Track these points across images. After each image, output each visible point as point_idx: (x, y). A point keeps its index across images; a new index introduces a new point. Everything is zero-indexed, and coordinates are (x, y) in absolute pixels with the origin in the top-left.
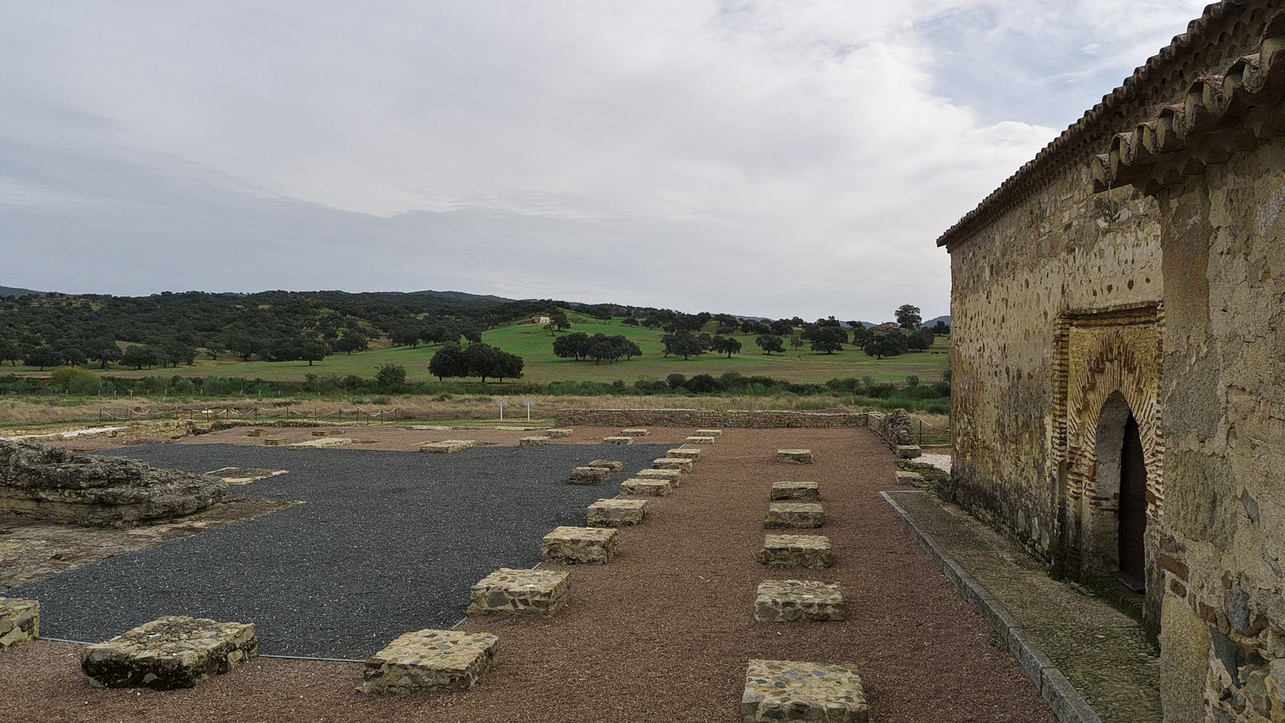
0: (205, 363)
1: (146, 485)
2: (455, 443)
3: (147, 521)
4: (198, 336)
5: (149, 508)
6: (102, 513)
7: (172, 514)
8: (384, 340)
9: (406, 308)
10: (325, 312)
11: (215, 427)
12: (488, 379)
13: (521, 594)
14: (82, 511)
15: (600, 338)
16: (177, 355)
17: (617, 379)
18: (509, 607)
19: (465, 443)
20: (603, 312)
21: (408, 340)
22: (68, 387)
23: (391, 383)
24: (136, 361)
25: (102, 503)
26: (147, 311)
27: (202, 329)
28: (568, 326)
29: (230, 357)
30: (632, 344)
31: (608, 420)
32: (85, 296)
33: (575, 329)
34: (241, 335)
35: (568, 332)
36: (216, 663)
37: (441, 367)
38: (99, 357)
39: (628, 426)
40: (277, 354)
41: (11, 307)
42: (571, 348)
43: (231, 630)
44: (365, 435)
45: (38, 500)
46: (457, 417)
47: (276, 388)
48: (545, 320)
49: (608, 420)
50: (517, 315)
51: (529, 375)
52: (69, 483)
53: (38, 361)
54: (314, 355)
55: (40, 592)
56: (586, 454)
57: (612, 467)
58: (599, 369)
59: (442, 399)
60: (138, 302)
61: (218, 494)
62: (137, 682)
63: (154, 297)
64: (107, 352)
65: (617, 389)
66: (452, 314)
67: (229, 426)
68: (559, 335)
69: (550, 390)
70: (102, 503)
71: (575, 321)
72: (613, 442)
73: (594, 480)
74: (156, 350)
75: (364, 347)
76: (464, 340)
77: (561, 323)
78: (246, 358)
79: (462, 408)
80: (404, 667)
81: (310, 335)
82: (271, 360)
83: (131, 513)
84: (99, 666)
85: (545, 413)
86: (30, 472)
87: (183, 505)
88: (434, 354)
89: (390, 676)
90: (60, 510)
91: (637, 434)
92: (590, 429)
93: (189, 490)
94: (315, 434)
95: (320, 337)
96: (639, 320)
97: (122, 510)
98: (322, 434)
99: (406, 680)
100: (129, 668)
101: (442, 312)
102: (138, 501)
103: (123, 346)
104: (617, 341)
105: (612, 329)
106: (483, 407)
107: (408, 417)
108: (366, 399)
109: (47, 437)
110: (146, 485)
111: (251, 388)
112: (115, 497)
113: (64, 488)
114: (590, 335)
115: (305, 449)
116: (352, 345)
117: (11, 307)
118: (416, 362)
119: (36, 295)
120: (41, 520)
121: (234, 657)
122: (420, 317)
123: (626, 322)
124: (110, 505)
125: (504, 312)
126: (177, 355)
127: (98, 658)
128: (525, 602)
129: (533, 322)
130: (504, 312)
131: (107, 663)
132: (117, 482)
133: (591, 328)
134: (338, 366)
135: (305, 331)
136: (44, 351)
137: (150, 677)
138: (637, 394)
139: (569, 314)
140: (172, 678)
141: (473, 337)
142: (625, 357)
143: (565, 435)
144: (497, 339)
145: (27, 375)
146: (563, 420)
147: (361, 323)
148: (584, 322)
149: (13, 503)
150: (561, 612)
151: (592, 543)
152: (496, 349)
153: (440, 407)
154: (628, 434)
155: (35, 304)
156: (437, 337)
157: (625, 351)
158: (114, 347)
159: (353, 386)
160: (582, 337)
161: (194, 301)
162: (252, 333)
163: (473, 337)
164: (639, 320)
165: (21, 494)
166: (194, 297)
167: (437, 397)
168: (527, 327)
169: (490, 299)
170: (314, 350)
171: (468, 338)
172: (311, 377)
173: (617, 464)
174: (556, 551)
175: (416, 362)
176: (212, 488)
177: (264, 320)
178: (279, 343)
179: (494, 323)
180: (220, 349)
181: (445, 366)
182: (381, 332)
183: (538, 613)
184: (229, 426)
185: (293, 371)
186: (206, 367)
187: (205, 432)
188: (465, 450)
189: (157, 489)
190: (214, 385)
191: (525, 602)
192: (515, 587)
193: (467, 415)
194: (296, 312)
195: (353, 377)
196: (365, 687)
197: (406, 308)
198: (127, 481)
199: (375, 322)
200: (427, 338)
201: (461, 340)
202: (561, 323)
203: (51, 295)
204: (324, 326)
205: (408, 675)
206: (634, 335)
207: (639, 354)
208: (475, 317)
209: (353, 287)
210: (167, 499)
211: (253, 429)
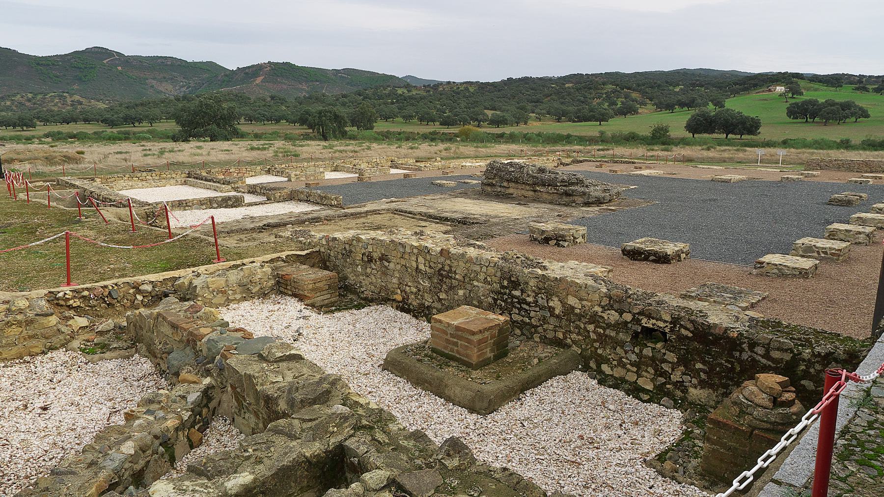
0: (535, 123)
1: (587, 186)
2: (735, 177)
3: (588, 204)
4: (529, 106)
5: (589, 198)
6: (566, 199)
7: (599, 202)
8: (649, 106)
9: (667, 82)
10: (610, 87)
11: (573, 162)
12: (730, 136)
13: (823, 248)
14: (556, 197)
15: (830, 103)
16: (519, 119)
17: (844, 138)
18: (815, 254)
19: (741, 177)
20: (835, 81)
21: (670, 107)
22: (466, 137)
23: (659, 138)
24: (497, 122)
25: (567, 194)
26: (499, 91)
27: (532, 102)
28: (801, 94)
29: (549, 120)
30: (861, 109)
31: (849, 167)
32: (464, 83)
33: (807, 96)
34: (556, 105)
35: (800, 99)
36: (677, 256)
37: (695, 127)
38: (477, 120)
39: (866, 172)
40: (578, 117)
41: (429, 91)
42: (803, 112)
43: (680, 246)
44: (669, 170)
45: (535, 191)
46: (725, 161)
47: (582, 140)
48: (780, 89)
49: (849, 167)
50: (755, 86)
51: (765, 133)
52: (551, 183)
53: (446, 123)
54: (602, 118)
55: (273, 289)
56: (841, 188)
57: (861, 197)
58: (827, 129)
59: (708, 149)
60: (494, 85)
61: (618, 194)
62: (646, 259)
63: (503, 81)
64: (481, 117)
65: (845, 145)
66: (702, 86)
67: (581, 162)
68: (793, 101)
69: (785, 144)
70: (567, 194)
71: (808, 89)
72: (856, 182)
73: (848, 203)
74: (507, 116)
75: (636, 112)
76: (711, 106)
77: (795, 91)
78: (559, 120)
79: (726, 155)
80: (776, 265)
81: (599, 104)
82: (574, 122)
83: (580, 200)
84: (629, 252)
85: (792, 161)
86: (533, 177)
87: (604, 198)
88: (690, 116)
89: (767, 268)
90: (545, 196)
91: (876, 178)
92: (833, 173)
93: (605, 191)
94: (636, 168)
95: (606, 105)
96: (870, 87)
97: (576, 198)
98: (640, 168)
99: (776, 271)
100: (643, 253)
101: (694, 85)
102: (584, 194)
103: (489, 113)
104: (846, 106)
105: (841, 95)
106: (741, 155)
107: (690, 160)
108: (656, 148)
109: (540, 162)
110: (587, 186)
111: (568, 139)
112: (573, 191)
113: (549, 185)
114: (822, 100)
115: (637, 176)
116: (627, 111)
117: (429, 91)
118: (677, 122)
119: (441, 84)
120: (536, 200)
121: (683, 256)
122: (677, 89)
123: (857, 89)
124: (570, 195)
125: (744, 83)
126: (519, 119)
127: (628, 248)
128: (826, 253)
129: (770, 91)
130: (744, 83)
131: (632, 251)
132: (573, 184)
133: (822, 95)
134: (618, 125)
135: (596, 102)
136: (448, 117)
137: (652, 258)
138: (864, 149)
139: (802, 83)
140: (662, 259)
141: (719, 104)
142: (853, 119)
143: (814, 176)
144: (738, 105)
145: (442, 131)
146: (810, 165)
147: (635, 95)
148: (816, 90)
149: (523, 192)
150: (844, 261)
151: (860, 233)
152: (739, 113)
153: (705, 154)
154: (868, 177)
155: (441, 89)
156: (690, 104)
157: (853, 114)
158: (484, 114)
159: (631, 139)
160: (813, 103)
161: (526, 83)
162: (562, 103)
163: (719, 104)
164: (870, 87)
165: (528, 188)
166: (526, 80)
167: (704, 147)
168: (766, 95)
169: (733, 74)
170: (603, 115)
171: (715, 105)
172: (602, 133)
173: (863, 195)
174: (834, 235)
175: (677, 122)
176: (616, 191)
177: (569, 94)
178: (579, 110)
179: (736, 93)
180: (543, 115)
181: (700, 126)
182: (648, 101)
183: (833, 259)
184: (581, 162)
185: (590, 129)
186: (534, 126)
187: (568, 165)
188: (742, 181)
189: (592, 188)
190: (549, 137)
191: (826, 253)
192: (818, 245)
193: (731, 160)
194: (590, 88)
195: (633, 133)
196: (754, 271)
197: (667, 82)
198: (577, 184)
199: (644, 93)
200: (682, 105)
201: (711, 105)
202: (795, 91)
203: (449, 83)
204: (608, 97)
205: (778, 269)
206: (862, 100)
207: (867, 116)
208: (720, 88)
209: (628, 69)
210: (597, 194)
211: (598, 164)
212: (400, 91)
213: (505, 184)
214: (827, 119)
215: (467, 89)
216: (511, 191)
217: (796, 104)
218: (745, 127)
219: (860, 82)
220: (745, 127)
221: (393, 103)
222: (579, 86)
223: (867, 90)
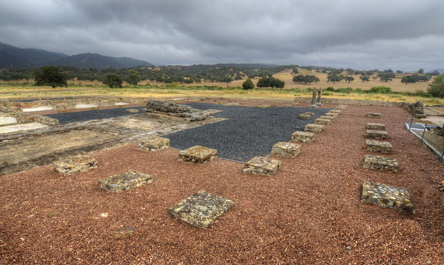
6: (182, 119)
30: (317, 78)
36: (207, 159)
51: (286, 87)
57: (311, 115)
102: (190, 116)
103: (185, 78)
132: (185, 111)
138: (372, 71)
141: (270, 76)
188: (269, 107)
212: (149, 68)
213: (155, 111)
214: (306, 82)
215: (177, 69)
216: (158, 115)
217: (296, 76)
218: (279, 85)
219: (317, 69)
220: (279, 85)
221: (146, 74)
222: (221, 68)
223: (319, 72)
